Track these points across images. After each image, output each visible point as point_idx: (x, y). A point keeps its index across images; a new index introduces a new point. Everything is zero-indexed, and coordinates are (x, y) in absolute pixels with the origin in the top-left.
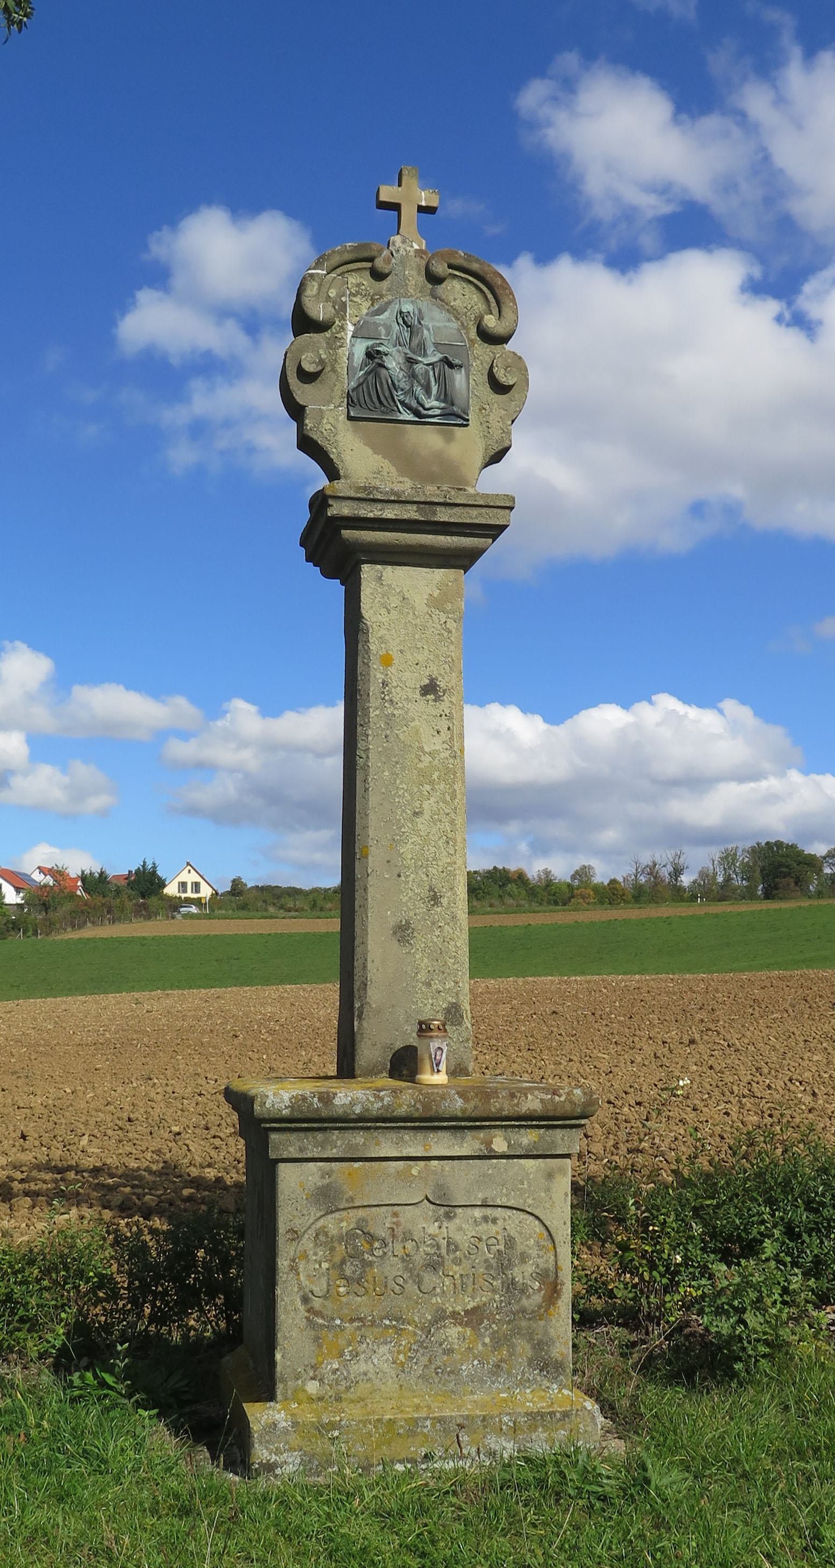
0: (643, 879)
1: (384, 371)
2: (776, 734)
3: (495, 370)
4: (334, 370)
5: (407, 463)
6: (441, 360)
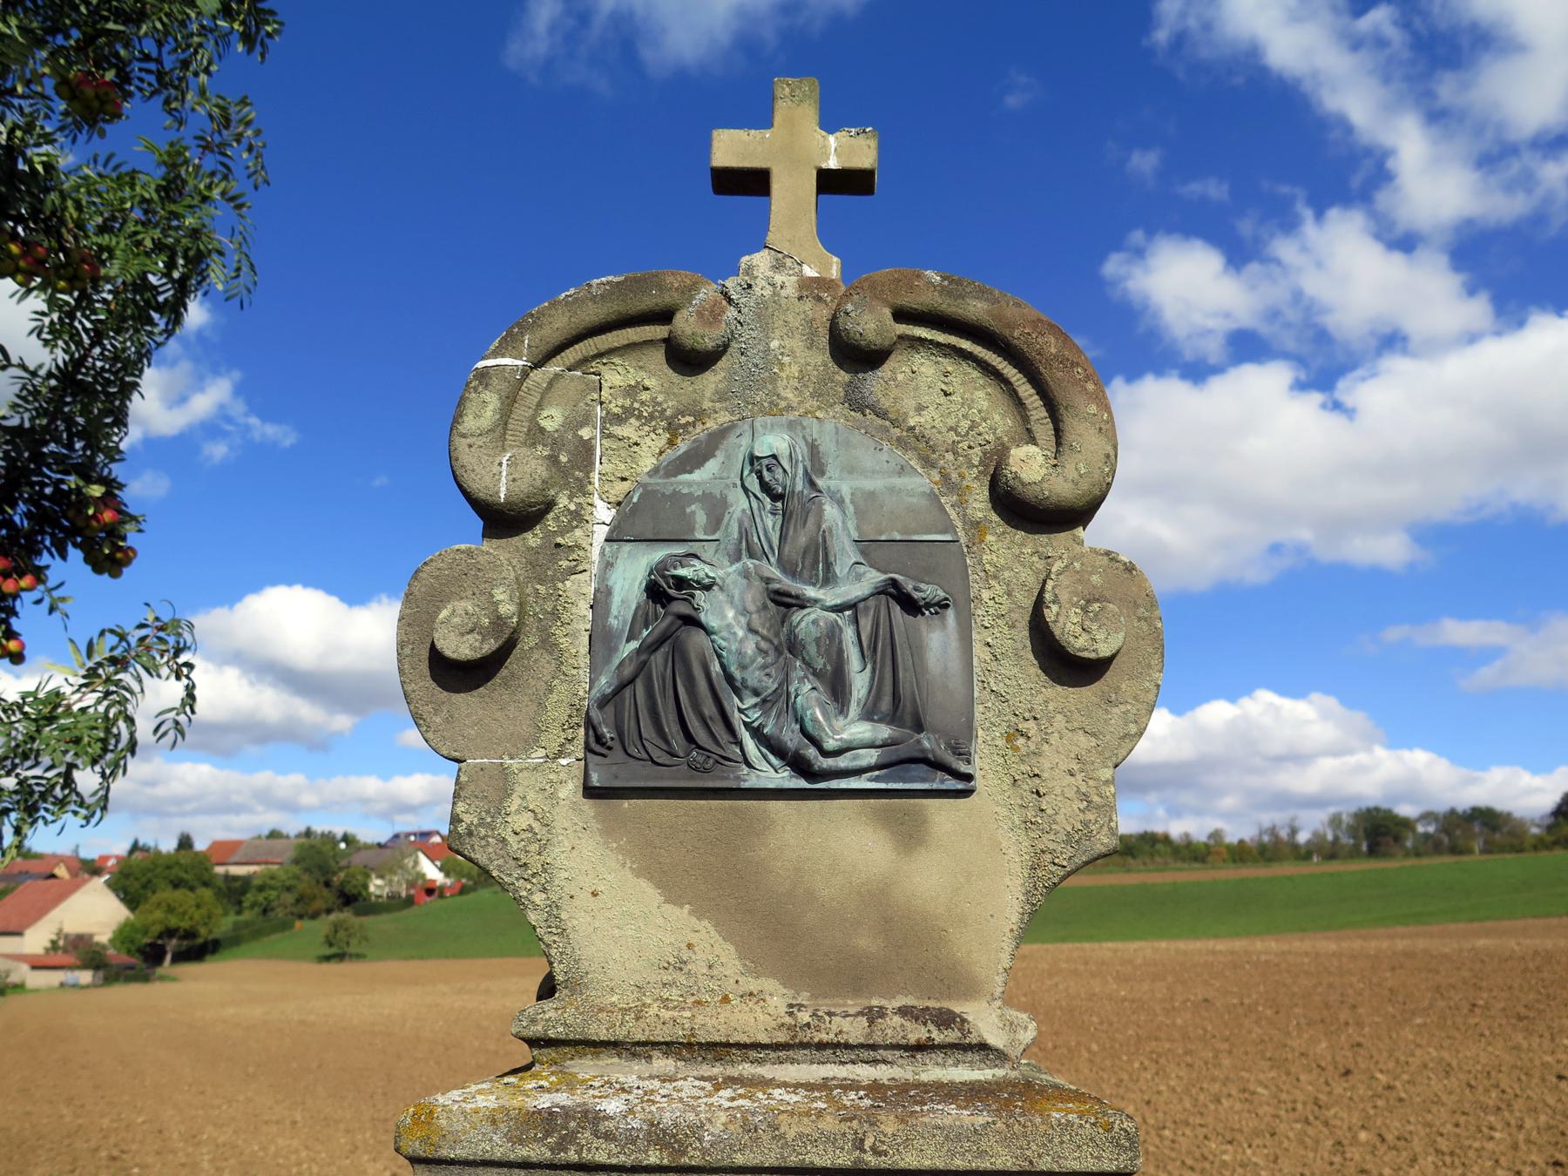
0: (1266, 838)
1: (697, 639)
2: (1359, 718)
3: (1050, 614)
4: (548, 644)
5: (773, 928)
6: (880, 592)
